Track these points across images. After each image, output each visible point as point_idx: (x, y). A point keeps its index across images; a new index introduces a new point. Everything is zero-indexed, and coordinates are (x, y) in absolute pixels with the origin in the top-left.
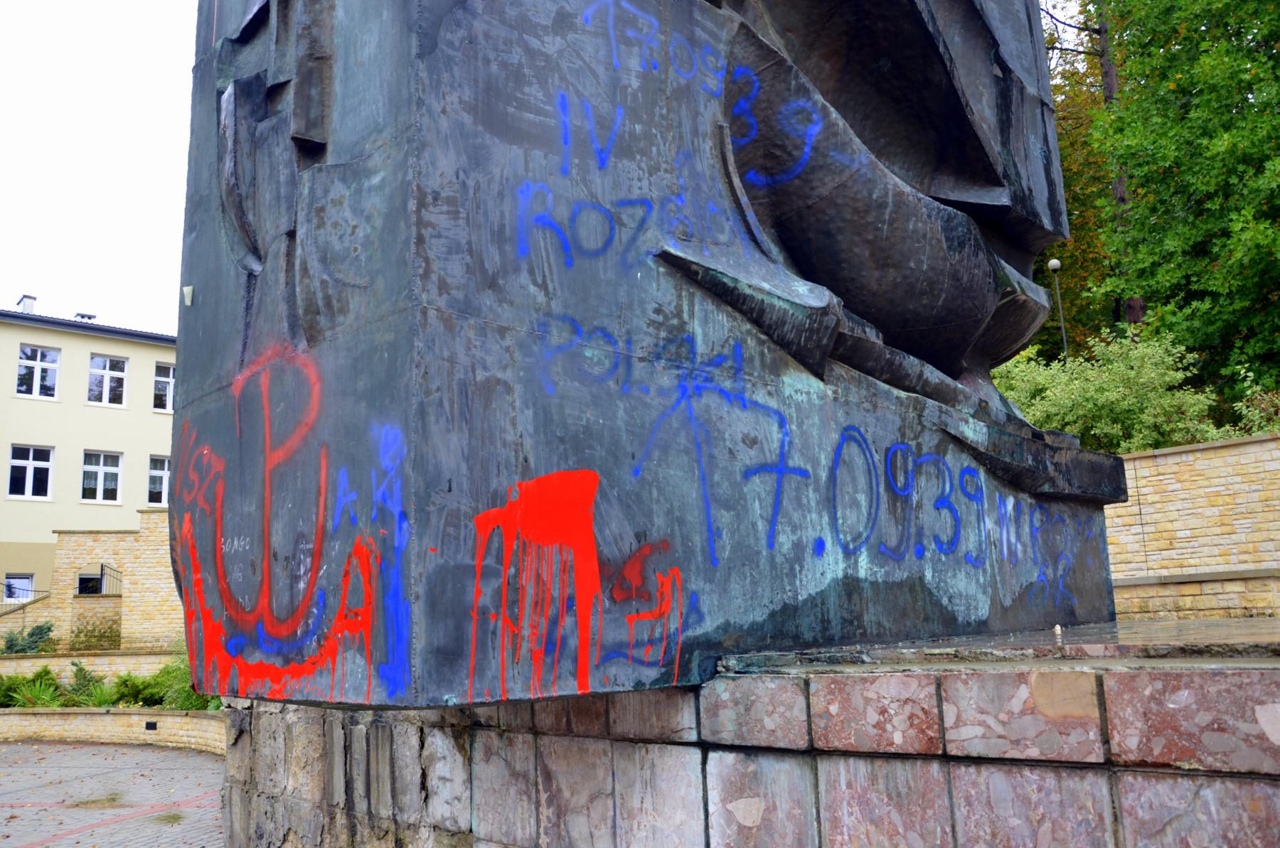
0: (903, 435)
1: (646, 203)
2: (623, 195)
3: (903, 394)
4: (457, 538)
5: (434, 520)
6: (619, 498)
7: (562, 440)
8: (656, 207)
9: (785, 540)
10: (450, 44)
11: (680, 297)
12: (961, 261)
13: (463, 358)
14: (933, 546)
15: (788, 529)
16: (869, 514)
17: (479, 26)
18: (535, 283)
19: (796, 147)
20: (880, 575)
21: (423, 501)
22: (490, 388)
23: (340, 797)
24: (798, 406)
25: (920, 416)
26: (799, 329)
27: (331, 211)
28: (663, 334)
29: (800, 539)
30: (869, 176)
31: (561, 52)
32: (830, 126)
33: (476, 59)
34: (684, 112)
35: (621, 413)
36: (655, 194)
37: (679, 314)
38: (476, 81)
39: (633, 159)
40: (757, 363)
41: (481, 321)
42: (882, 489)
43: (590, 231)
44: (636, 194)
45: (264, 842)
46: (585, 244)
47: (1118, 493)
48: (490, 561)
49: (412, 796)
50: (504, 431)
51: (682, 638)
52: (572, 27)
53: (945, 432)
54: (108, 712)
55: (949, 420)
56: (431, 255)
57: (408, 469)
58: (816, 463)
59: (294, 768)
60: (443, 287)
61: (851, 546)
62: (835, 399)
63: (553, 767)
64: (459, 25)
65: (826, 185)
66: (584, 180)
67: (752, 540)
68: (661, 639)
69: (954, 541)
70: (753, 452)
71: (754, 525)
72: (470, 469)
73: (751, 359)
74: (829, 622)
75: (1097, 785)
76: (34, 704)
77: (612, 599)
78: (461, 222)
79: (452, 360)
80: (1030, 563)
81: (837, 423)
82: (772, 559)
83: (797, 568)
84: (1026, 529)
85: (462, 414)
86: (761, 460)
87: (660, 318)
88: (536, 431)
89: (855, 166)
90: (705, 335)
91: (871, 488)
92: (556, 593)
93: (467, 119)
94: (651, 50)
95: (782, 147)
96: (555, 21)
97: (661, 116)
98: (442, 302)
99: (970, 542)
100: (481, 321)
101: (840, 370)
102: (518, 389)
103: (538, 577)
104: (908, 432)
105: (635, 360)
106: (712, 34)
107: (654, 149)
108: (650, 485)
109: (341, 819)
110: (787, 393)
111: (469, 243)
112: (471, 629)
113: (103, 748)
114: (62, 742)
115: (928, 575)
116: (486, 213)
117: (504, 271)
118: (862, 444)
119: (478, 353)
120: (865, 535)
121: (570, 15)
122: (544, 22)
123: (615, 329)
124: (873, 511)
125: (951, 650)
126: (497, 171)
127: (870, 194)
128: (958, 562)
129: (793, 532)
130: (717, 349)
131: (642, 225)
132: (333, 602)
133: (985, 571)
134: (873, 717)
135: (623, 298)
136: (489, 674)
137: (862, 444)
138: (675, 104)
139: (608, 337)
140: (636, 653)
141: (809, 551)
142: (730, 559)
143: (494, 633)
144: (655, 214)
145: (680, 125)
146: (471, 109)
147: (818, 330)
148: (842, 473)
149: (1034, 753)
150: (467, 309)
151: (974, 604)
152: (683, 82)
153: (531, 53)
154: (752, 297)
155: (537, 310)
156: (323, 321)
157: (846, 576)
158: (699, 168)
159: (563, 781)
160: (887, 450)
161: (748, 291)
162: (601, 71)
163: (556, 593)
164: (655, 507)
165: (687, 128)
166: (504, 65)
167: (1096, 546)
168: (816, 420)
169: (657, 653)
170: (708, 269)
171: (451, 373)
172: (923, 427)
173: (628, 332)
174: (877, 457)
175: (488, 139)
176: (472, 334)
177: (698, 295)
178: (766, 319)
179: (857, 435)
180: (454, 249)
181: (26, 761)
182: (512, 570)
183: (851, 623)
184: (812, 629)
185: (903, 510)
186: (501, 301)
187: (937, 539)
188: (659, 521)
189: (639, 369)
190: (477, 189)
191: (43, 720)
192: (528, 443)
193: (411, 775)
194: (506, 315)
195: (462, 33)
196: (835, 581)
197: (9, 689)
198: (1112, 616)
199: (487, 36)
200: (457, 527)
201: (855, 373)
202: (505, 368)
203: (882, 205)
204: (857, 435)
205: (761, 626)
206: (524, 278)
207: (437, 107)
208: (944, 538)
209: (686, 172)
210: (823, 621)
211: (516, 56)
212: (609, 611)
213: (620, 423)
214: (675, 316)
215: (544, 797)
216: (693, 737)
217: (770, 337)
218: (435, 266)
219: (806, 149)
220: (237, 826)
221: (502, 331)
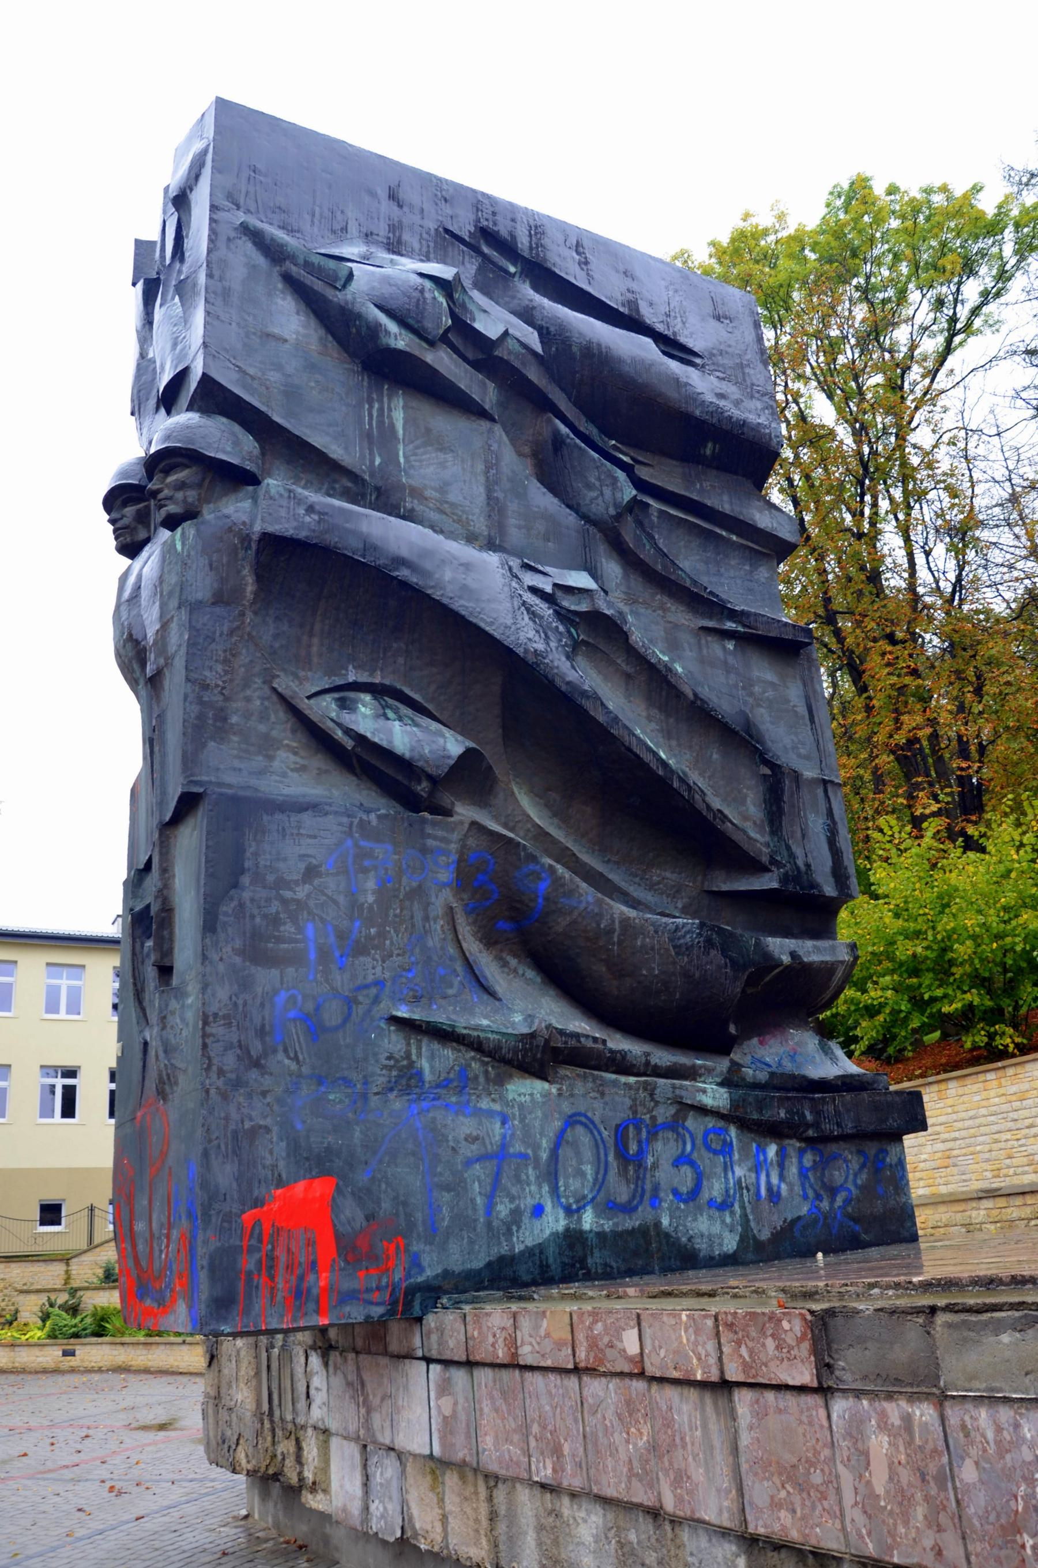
0: (635, 1112)
1: (379, 983)
2: (359, 982)
3: (632, 1079)
4: (230, 1229)
5: (214, 1220)
6: (353, 1194)
7: (307, 1159)
8: (388, 984)
9: (503, 1209)
10: (226, 914)
11: (408, 1044)
12: (690, 961)
13: (235, 1116)
14: (671, 1197)
15: (506, 1200)
16: (596, 1180)
17: (246, 895)
18: (289, 1058)
19: (531, 900)
20: (608, 1226)
21: (207, 1208)
22: (253, 1133)
23: (265, 1407)
24: (521, 1106)
25: (652, 1095)
26: (516, 1051)
27: (170, 1018)
28: (394, 1073)
29: (518, 1207)
30: (596, 910)
31: (308, 896)
32: (558, 881)
33: (244, 917)
34: (416, 906)
35: (357, 1134)
36: (387, 975)
37: (408, 1055)
38: (244, 933)
39: (369, 954)
40: (482, 1079)
41: (248, 1090)
42: (611, 1157)
43: (332, 1014)
44: (370, 978)
45: (226, 1446)
46: (328, 1024)
47: (919, 1124)
48: (253, 1242)
49: (302, 1404)
50: (263, 1158)
51: (404, 1285)
52: (319, 875)
53: (681, 1103)
54: (184, 1342)
55: (683, 1093)
56: (212, 1054)
57: (197, 1190)
58: (536, 1147)
59: (242, 1385)
60: (221, 1072)
61: (574, 1207)
62: (560, 1095)
63: (365, 1378)
64: (232, 899)
65: (561, 924)
66: (327, 981)
67: (470, 1212)
68: (387, 1286)
69: (695, 1193)
70: (474, 1147)
71: (473, 1200)
72: (239, 1185)
73: (476, 1077)
74: (548, 1266)
75: (572, 1382)
76: (123, 1334)
77: (347, 1262)
78: (234, 1029)
79: (227, 1118)
80: (797, 1200)
81: (560, 1113)
82: (489, 1225)
83: (514, 1228)
84: (793, 1170)
85: (234, 1152)
86: (483, 1151)
87: (392, 1062)
88: (288, 1155)
89: (583, 906)
90: (432, 1067)
91: (599, 1159)
92: (302, 1259)
93: (238, 960)
94: (386, 869)
95: (521, 902)
96: (304, 875)
97: (395, 916)
98: (220, 1083)
99: (715, 1189)
100: (248, 1090)
101: (565, 1071)
102: (275, 1129)
103: (289, 1251)
104: (639, 1109)
105: (370, 1096)
106: (443, 839)
107: (388, 942)
108: (380, 1181)
109: (267, 1425)
110: (510, 1097)
111: (239, 1041)
112: (240, 1286)
113: (180, 1378)
114: (147, 1371)
115: (665, 1221)
116: (251, 1020)
117: (265, 1054)
118: (590, 1125)
119: (245, 1111)
120: (590, 1196)
121: (316, 867)
122: (295, 878)
123: (354, 1076)
124: (600, 1177)
125: (572, 1291)
126: (259, 990)
127: (598, 925)
128: (700, 1209)
129: (511, 1201)
130: (443, 1076)
131: (376, 1000)
132: (174, 1267)
133: (732, 1213)
134: (491, 1340)
135: (359, 1054)
136: (253, 1313)
137: (590, 1125)
138: (407, 903)
139: (347, 1082)
140: (365, 1296)
141: (527, 1214)
142: (448, 1227)
143: (257, 1287)
144: (387, 990)
145: (412, 917)
146: (241, 952)
147: (531, 1049)
148: (564, 1152)
149: (549, 1363)
150: (238, 1084)
151: (717, 1241)
152: (415, 884)
153: (284, 902)
154: (469, 1035)
155: (290, 1075)
156: (167, 1087)
157: (567, 1230)
158: (430, 944)
159: (369, 1388)
160: (618, 1126)
161: (464, 1032)
162: (341, 899)
163: (302, 1259)
164: (382, 1196)
165: (419, 916)
166: (265, 916)
167: (896, 1177)
168: (539, 1114)
169: (386, 1296)
170: (428, 1022)
171: (226, 1127)
172: (657, 1103)
173: (365, 1077)
174: (605, 1133)
175: (253, 969)
176: (241, 1099)
177: (425, 1041)
178: (485, 1047)
179: (583, 1119)
180: (229, 1047)
181: (112, 1389)
182: (270, 1247)
183: (573, 1266)
184: (528, 1272)
185: (636, 1171)
186: (263, 1075)
187: (676, 1192)
188: (386, 1205)
189: (374, 1101)
190: (245, 1004)
191: (130, 1349)
192: (282, 1164)
193: (301, 1388)
194: (267, 1082)
195: (235, 903)
196: (555, 1235)
197: (103, 1319)
198: (914, 1238)
199: (252, 900)
200: (230, 1222)
201: (580, 1071)
202: (265, 1117)
203: (610, 932)
204: (583, 1119)
205: (479, 1272)
206: (280, 1056)
207: (216, 957)
208: (684, 1190)
209: (417, 950)
210: (541, 1266)
211: (275, 907)
212: (344, 1269)
213: (357, 1141)
214: (403, 1059)
215: (361, 1399)
216: (420, 1353)
217: (494, 1058)
218: (215, 1061)
219: (540, 900)
220: (211, 1434)
221: (264, 1094)
